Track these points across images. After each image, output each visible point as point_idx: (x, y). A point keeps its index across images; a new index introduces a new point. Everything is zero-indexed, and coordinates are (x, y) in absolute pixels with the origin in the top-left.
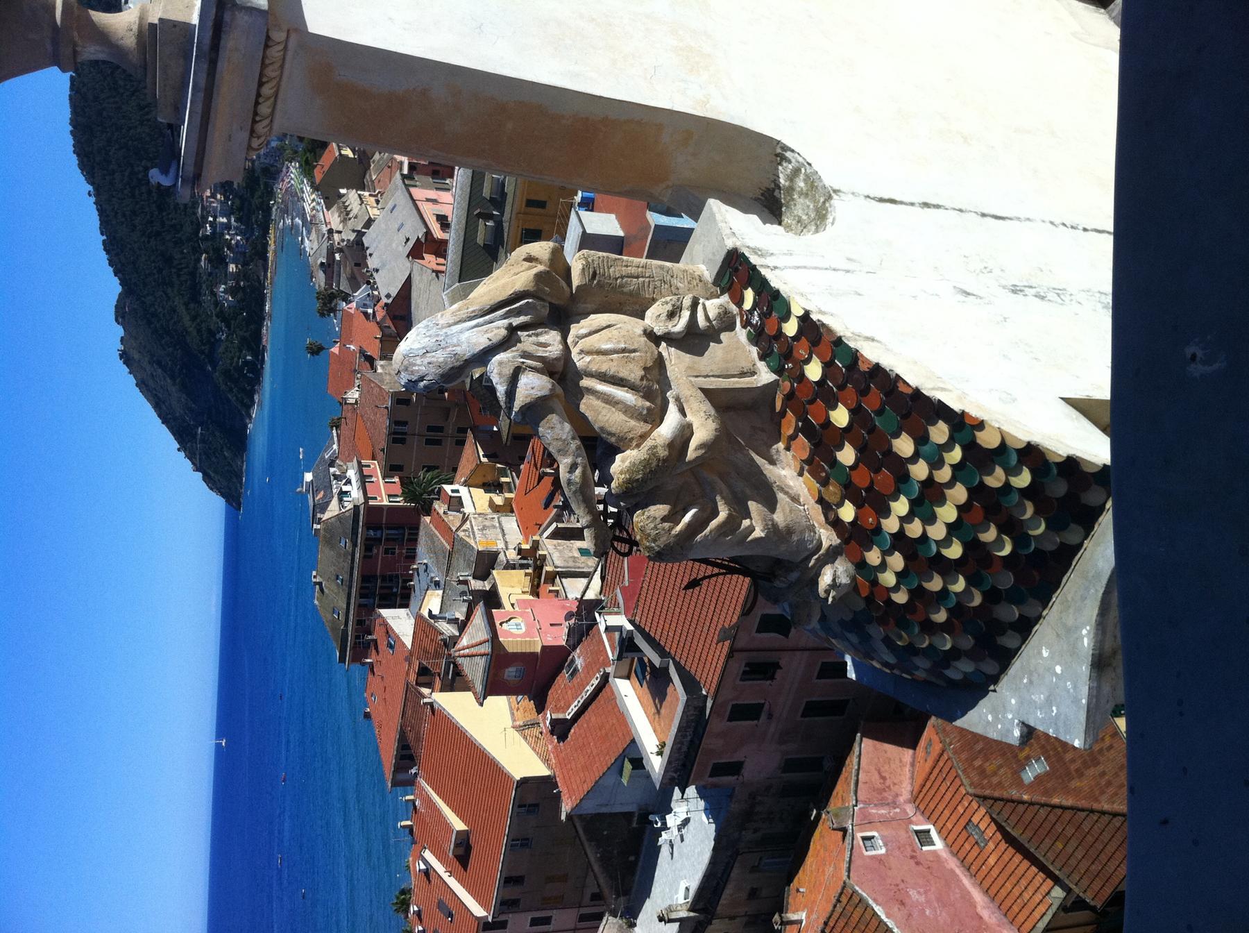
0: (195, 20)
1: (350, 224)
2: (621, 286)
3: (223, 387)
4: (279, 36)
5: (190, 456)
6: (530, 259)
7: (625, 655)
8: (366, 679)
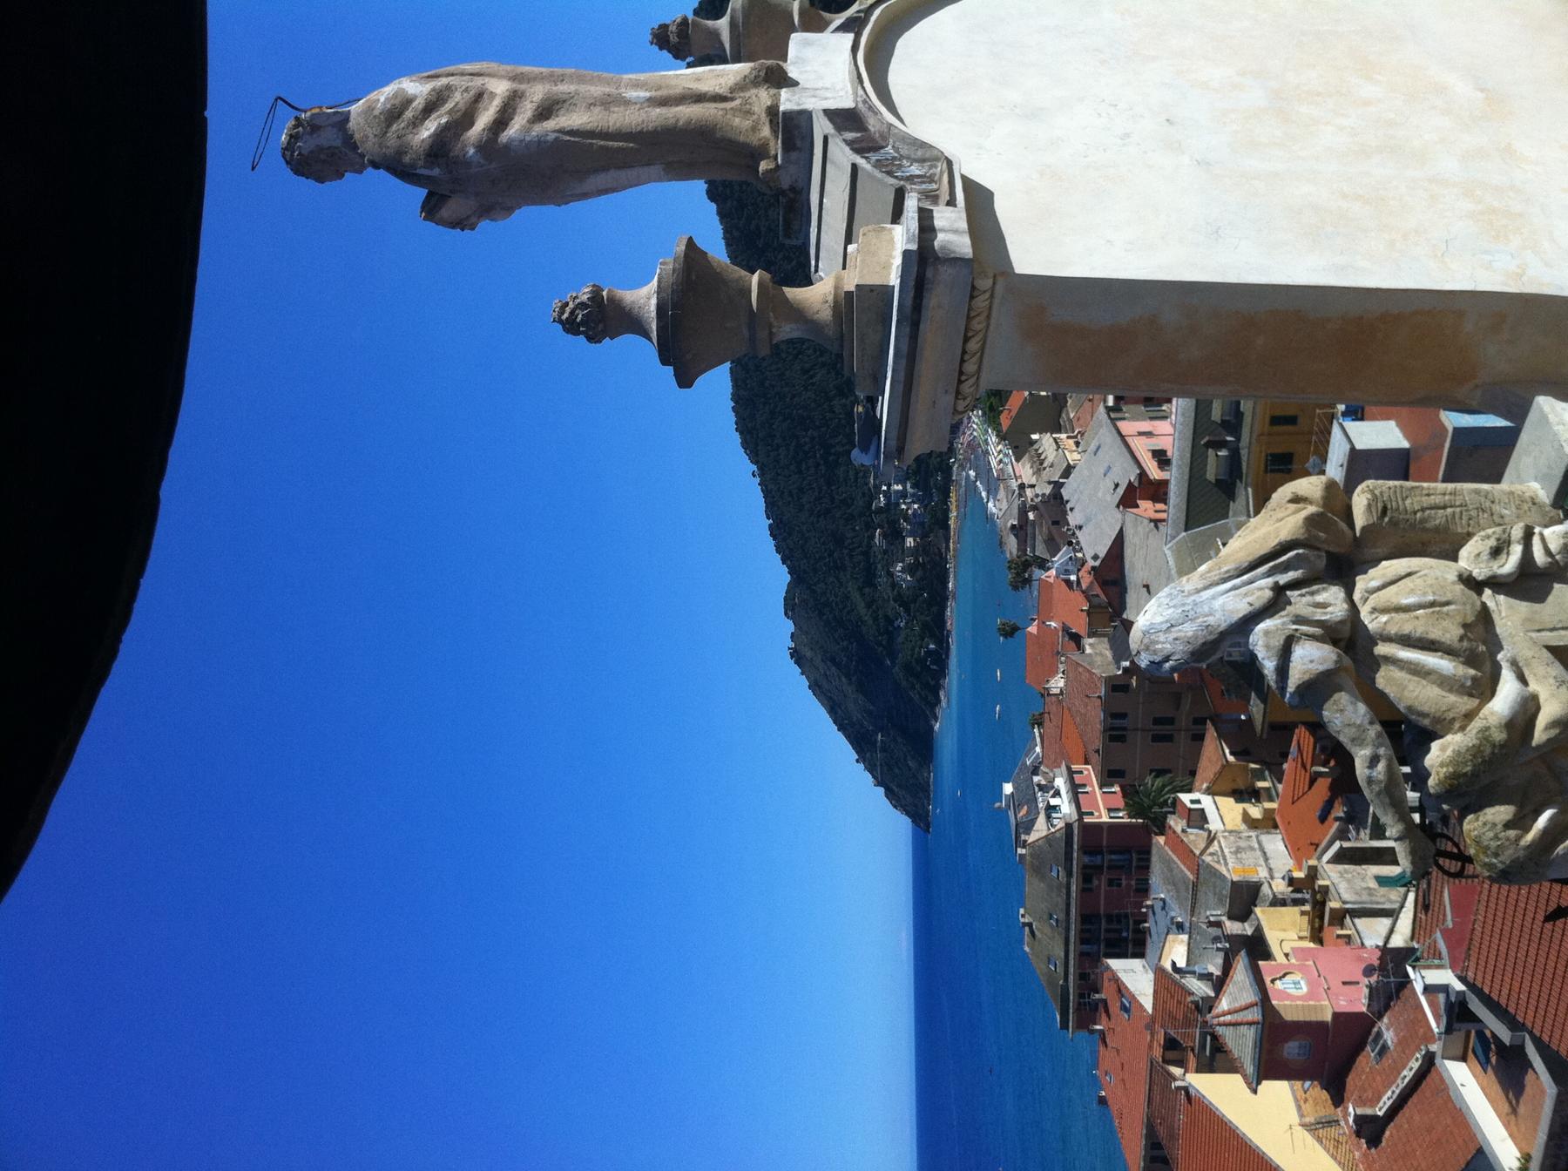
0: (894, 280)
1: (1045, 475)
2: (1423, 521)
3: (904, 683)
4: (984, 284)
5: (871, 769)
6: (1297, 500)
7: (1456, 1026)
8: (1095, 1054)
